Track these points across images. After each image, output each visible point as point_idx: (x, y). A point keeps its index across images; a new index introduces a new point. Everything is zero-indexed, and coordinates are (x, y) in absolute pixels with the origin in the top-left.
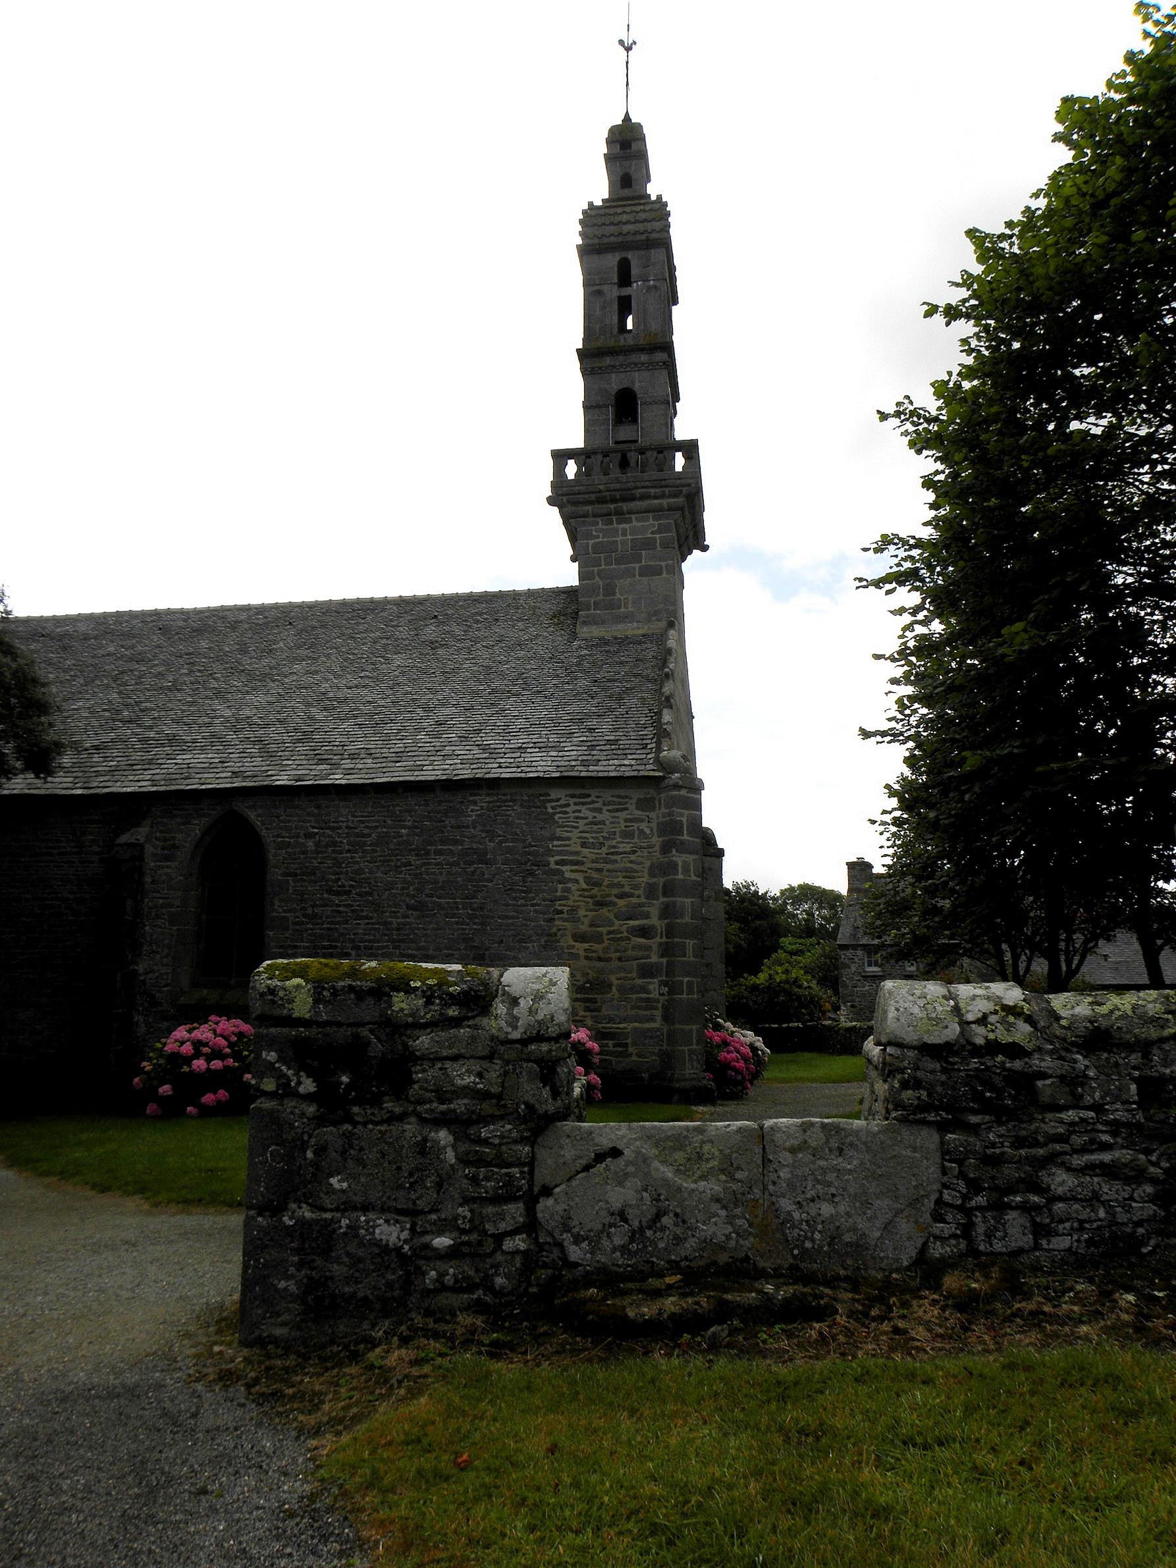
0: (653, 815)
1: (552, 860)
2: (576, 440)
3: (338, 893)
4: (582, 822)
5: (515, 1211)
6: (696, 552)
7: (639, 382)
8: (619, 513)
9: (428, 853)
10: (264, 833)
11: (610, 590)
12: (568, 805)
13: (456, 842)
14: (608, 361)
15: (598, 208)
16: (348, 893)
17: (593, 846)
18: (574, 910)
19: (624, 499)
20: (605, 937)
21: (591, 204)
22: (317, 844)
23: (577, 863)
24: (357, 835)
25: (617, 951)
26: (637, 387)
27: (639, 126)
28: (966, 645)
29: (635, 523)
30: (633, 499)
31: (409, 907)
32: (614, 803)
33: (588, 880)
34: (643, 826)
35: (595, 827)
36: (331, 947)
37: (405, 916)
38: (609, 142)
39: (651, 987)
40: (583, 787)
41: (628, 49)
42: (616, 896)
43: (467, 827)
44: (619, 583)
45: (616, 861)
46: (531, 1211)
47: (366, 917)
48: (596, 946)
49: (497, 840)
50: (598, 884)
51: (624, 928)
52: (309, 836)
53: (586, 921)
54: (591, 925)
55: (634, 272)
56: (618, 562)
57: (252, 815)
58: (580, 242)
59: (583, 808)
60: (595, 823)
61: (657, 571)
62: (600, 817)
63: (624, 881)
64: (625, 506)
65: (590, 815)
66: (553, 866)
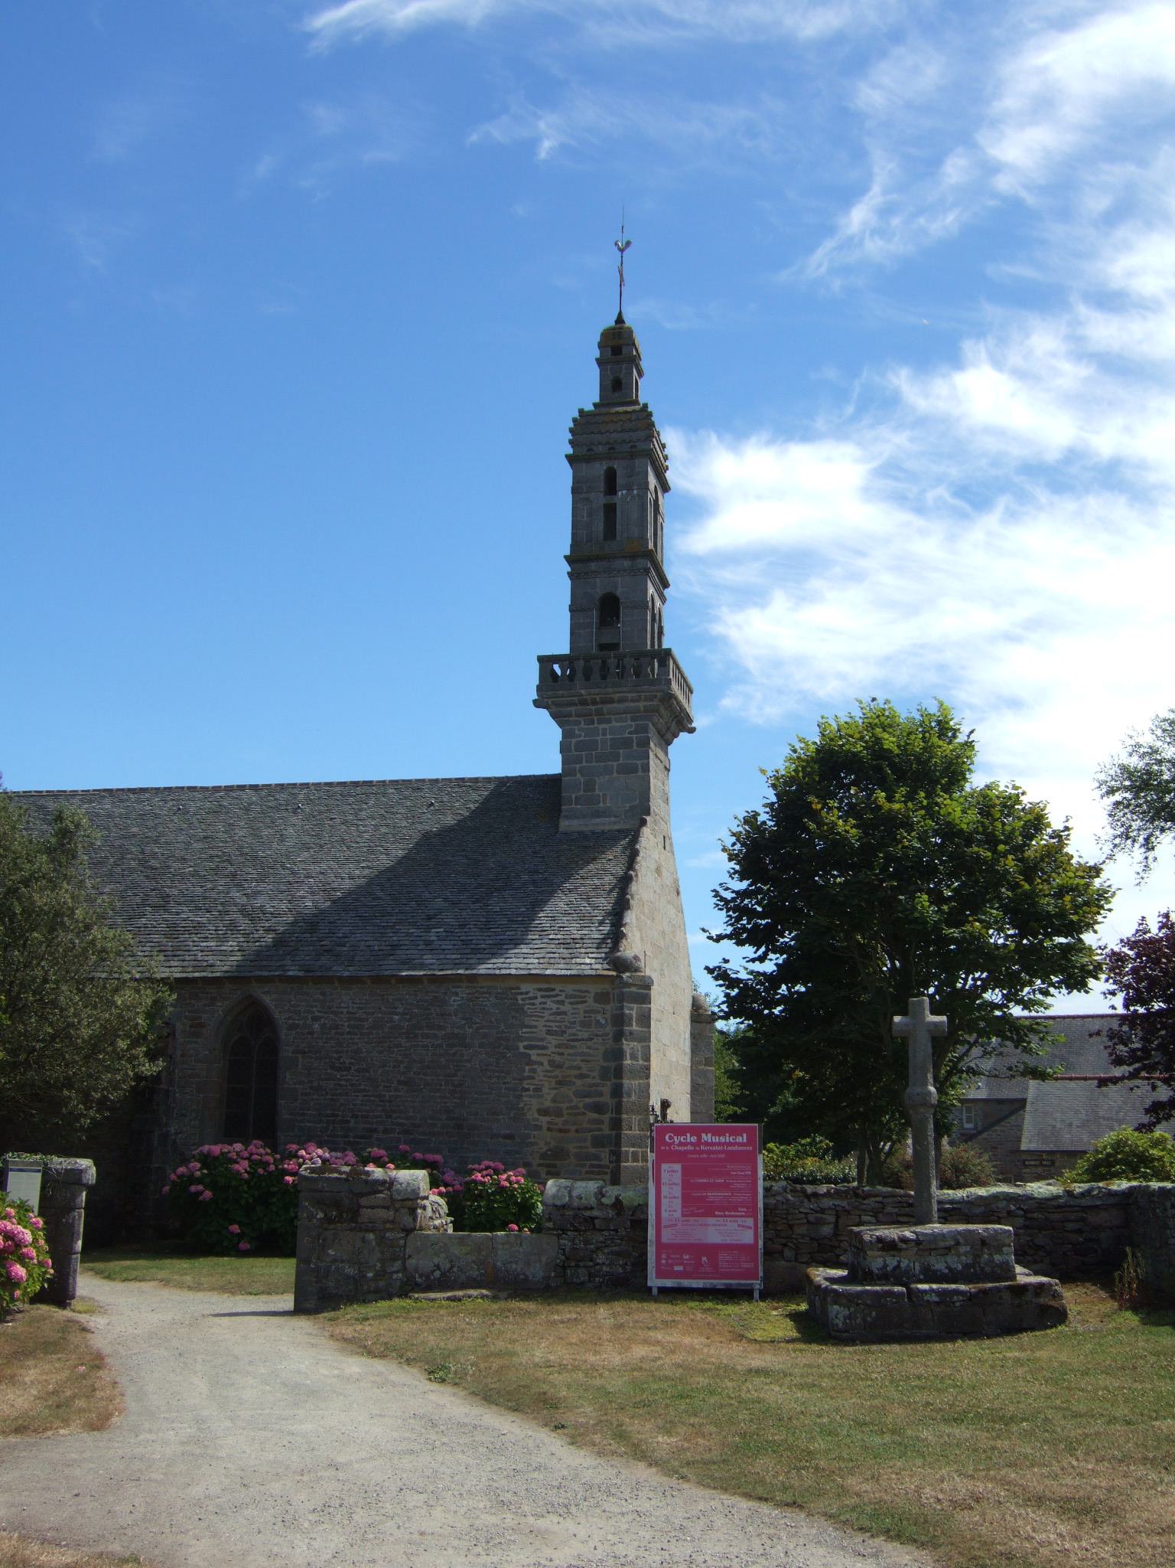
0: (608, 1007)
1: (521, 1045)
2: (563, 648)
3: (339, 1069)
4: (547, 1013)
5: (398, 1264)
6: (683, 735)
8: (599, 713)
11: (590, 786)
13: (440, 1028)
14: (593, 566)
16: (348, 1069)
17: (556, 1033)
18: (538, 1089)
19: (603, 702)
20: (565, 1112)
21: (581, 411)
23: (544, 1048)
26: (619, 592)
27: (630, 331)
29: (614, 724)
30: (612, 701)
31: (399, 1082)
32: (574, 997)
33: (551, 1063)
34: (599, 1017)
35: (558, 1018)
37: (396, 1090)
41: (622, 251)
43: (449, 1015)
46: (404, 1264)
48: (557, 1120)
50: (559, 1066)
51: (581, 1105)
54: (554, 1101)
55: (619, 481)
57: (267, 999)
58: (570, 451)
59: (549, 1001)
60: (559, 1014)
62: (562, 1008)
63: (582, 1065)
64: (606, 708)
65: (554, 1006)
66: (522, 1050)
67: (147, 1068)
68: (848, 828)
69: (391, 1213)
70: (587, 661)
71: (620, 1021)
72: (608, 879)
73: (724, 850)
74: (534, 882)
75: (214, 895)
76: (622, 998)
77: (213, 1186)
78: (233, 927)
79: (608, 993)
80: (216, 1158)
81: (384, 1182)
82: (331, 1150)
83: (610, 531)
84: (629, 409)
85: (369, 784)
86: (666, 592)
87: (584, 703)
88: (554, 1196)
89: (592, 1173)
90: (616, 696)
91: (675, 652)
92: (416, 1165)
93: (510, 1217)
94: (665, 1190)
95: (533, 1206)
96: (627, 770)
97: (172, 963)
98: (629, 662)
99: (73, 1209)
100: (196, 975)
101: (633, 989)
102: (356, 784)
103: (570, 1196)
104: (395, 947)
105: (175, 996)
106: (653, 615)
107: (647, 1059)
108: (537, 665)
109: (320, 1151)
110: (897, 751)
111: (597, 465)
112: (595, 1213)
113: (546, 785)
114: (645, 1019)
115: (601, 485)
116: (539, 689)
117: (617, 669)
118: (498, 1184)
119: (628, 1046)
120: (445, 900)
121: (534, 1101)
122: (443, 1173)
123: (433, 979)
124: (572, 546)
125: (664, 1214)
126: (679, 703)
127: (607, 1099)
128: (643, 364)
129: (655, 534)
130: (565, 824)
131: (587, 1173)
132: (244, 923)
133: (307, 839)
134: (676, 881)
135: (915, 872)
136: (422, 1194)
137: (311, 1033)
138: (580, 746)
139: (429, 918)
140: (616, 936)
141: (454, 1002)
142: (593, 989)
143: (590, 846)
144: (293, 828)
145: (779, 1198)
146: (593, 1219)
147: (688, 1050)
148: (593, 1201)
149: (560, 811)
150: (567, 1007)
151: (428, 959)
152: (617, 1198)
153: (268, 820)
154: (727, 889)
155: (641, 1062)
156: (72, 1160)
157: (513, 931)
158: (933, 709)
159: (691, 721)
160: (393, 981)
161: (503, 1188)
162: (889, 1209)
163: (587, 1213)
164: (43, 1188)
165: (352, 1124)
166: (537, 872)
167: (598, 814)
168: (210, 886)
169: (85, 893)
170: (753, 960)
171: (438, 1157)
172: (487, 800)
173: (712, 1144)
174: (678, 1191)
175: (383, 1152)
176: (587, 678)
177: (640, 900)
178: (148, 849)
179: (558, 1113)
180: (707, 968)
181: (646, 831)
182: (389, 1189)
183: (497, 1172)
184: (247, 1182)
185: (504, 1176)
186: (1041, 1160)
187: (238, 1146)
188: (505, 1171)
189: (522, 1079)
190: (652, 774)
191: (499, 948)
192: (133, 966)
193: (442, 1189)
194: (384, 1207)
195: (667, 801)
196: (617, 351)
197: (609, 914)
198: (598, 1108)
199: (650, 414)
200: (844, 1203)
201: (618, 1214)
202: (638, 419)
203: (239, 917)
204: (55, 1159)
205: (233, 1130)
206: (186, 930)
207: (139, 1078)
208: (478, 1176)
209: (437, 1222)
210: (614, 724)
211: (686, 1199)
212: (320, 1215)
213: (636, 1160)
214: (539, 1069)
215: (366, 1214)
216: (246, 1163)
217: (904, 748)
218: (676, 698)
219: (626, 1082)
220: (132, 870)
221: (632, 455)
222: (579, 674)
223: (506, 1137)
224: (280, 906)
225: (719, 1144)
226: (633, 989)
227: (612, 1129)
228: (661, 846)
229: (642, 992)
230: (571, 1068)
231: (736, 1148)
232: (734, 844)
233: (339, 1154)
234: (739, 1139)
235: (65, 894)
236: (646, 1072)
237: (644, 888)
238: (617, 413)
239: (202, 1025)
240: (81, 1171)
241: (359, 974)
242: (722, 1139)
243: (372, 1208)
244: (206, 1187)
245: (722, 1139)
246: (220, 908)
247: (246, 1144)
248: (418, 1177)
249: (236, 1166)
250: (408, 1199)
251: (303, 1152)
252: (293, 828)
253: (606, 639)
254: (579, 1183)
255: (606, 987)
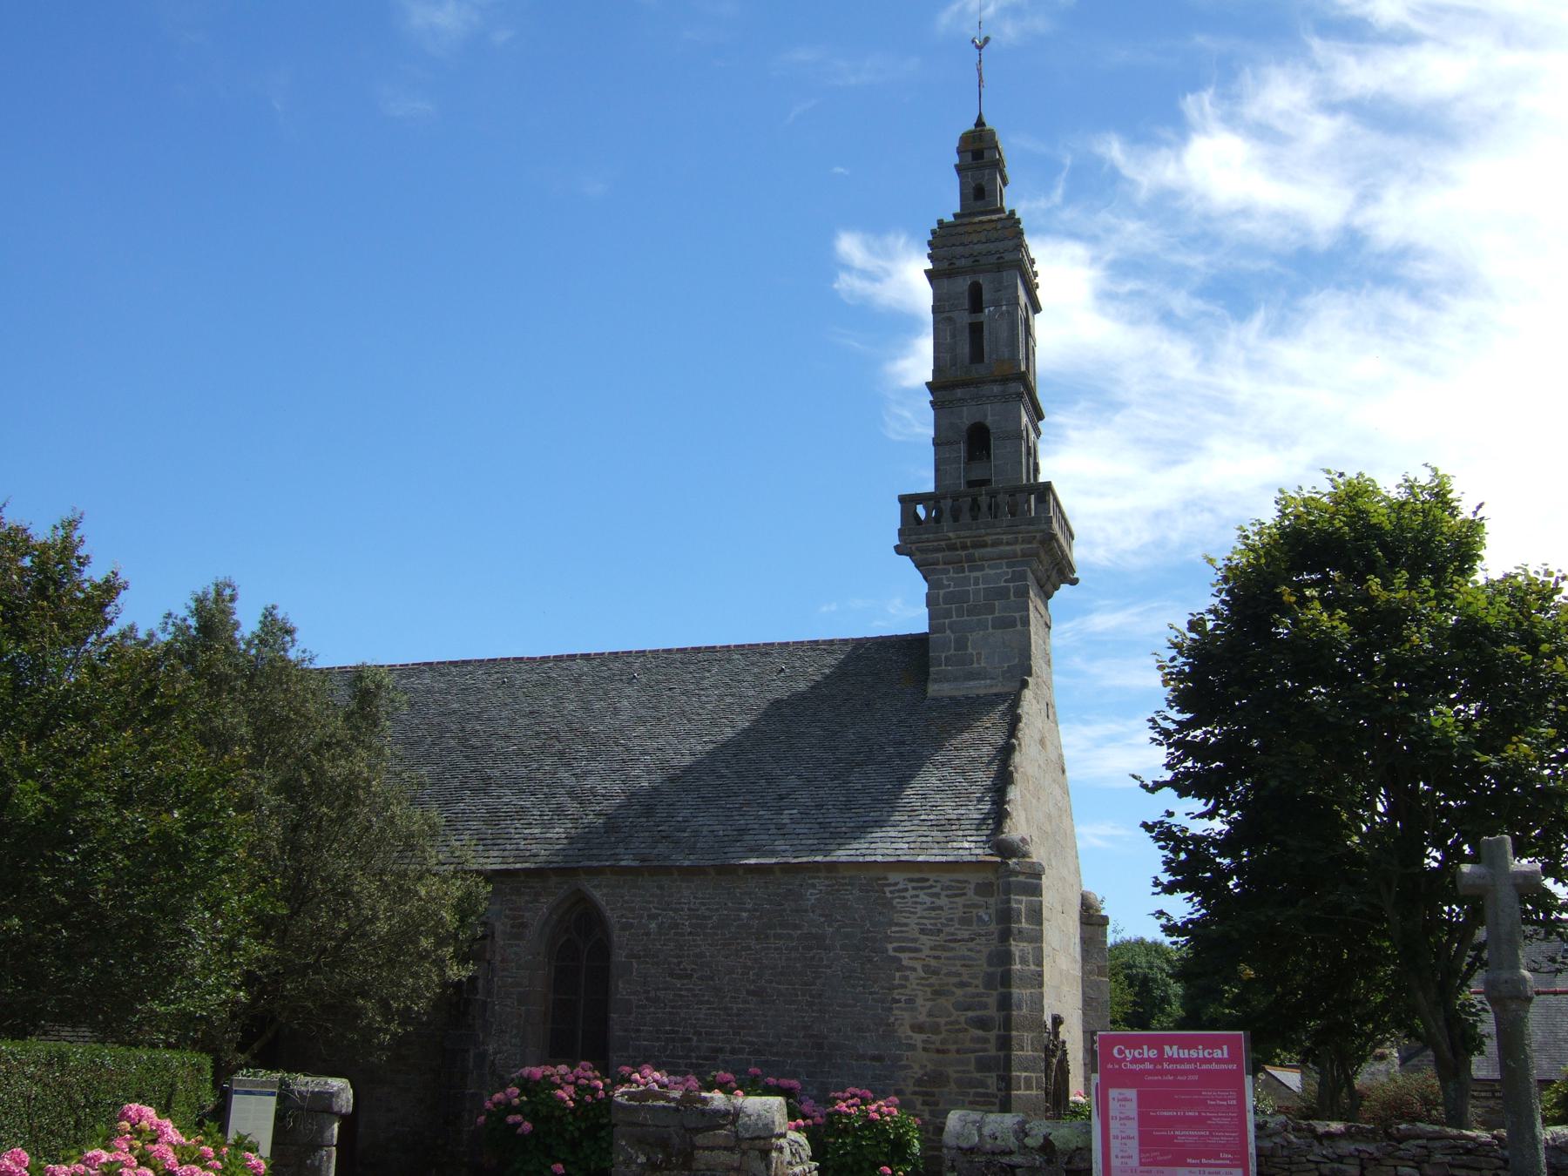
0: (992, 901)
1: (890, 947)
3: (680, 977)
7: (991, 416)
8: (970, 559)
9: (767, 937)
10: (608, 914)
11: (961, 644)
12: (906, 890)
13: (796, 927)
14: (959, 392)
15: (950, 225)
18: (910, 1001)
19: (976, 546)
20: (943, 1028)
21: (940, 222)
22: (660, 926)
23: (917, 950)
24: (698, 917)
25: (955, 1042)
26: (989, 421)
27: (992, 133)
28: (1358, 681)
30: (985, 545)
31: (749, 993)
33: (926, 968)
34: (981, 913)
35: (933, 914)
36: (673, 1032)
38: (960, 151)
39: (989, 1082)
40: (921, 871)
41: (979, 48)
42: (955, 985)
44: (972, 637)
45: (953, 949)
47: (708, 1002)
49: (836, 925)
50: (936, 972)
51: (962, 1019)
52: (652, 917)
53: (924, 1011)
54: (930, 1015)
55: (986, 296)
56: (970, 612)
58: (930, 266)
60: (933, 909)
61: (1012, 624)
62: (938, 902)
63: (963, 970)
64: (977, 553)
65: (928, 900)
66: (891, 953)
67: (455, 972)
68: (1336, 625)
69: (737, 1157)
70: (955, 498)
71: (1006, 916)
72: (986, 749)
73: (1161, 668)
74: (901, 755)
75: (539, 775)
76: (1008, 889)
77: (533, 1116)
78: (560, 811)
79: (991, 884)
80: (537, 1082)
81: (727, 1113)
82: (670, 1073)
83: (977, 354)
84: (994, 217)
85: (712, 649)
86: (1041, 424)
87: (952, 548)
88: (958, 1136)
89: (977, 1103)
90: (989, 539)
91: (1056, 487)
92: (769, 1091)
93: (882, 1158)
94: (1115, 1127)
95: (909, 1144)
96: (1005, 624)
97: (492, 853)
98: (1002, 498)
99: (321, 1147)
100: (518, 866)
101: (1021, 878)
102: (697, 650)
103: (981, 1135)
104: (743, 831)
105: (490, 888)
106: (1028, 448)
107: (1040, 964)
108: (899, 506)
109: (657, 1075)
110: (1389, 527)
111: (960, 280)
112: (1017, 1159)
113: (910, 650)
114: (1036, 915)
115: (966, 304)
116: (901, 533)
117: (985, 512)
118: (865, 1116)
119: (1017, 947)
120: (799, 777)
121: (906, 1015)
122: (801, 1102)
123: (787, 868)
124: (934, 371)
125: (1115, 1162)
126: (1060, 546)
127: (992, 1012)
128: (1007, 171)
129: (1027, 358)
130: (933, 689)
131: (971, 1103)
132: (572, 807)
133: (643, 712)
134: (1061, 756)
135: (1429, 680)
136: (777, 1130)
137: (648, 934)
138: (949, 598)
139: (781, 798)
140: (999, 814)
141: (811, 896)
142: (975, 878)
143: (964, 712)
144: (628, 700)
145: (1277, 1140)
146: (1013, 1167)
147: (1079, 958)
148: (1012, 1142)
149: (927, 673)
150: (943, 901)
151: (780, 845)
152: (1046, 1138)
153: (600, 692)
154: (1166, 718)
155: (1033, 967)
156: (322, 1080)
157: (877, 809)
158: (1424, 478)
159: (1073, 571)
160: (741, 872)
161: (873, 1121)
162: (1438, 1157)
163: (1005, 1160)
164: (280, 1117)
165: (694, 1043)
166: (903, 743)
167: (972, 676)
168: (535, 766)
169: (384, 769)
170: (1202, 816)
171: (794, 1083)
172: (844, 663)
173: (1180, 1061)
174: (1133, 1128)
175: (729, 1076)
176: (956, 519)
177: (1025, 774)
178: (469, 727)
179: (935, 1029)
180: (1145, 825)
181: (1028, 694)
182: (734, 1123)
183: (864, 1101)
184: (573, 1111)
185: (874, 1107)
186: (1493, 1092)
187: (563, 1069)
188: (874, 1101)
189: (892, 988)
190: (1032, 629)
191: (861, 830)
192: (445, 856)
193: (801, 1122)
194: (725, 1148)
195: (1048, 663)
196: (978, 155)
197: (988, 790)
198: (983, 1024)
199: (1018, 222)
200: (1371, 1148)
201: (1049, 1161)
202: (1004, 228)
203: (565, 799)
204: (301, 1078)
205: (560, 1050)
206: (508, 816)
207: (445, 984)
208: (842, 1106)
209: (798, 1169)
210: (987, 571)
211: (1146, 1140)
212: (642, 1159)
213: (1029, 1087)
214: (912, 976)
215: (703, 1156)
216: (571, 1089)
217: (1399, 526)
218: (1057, 541)
219: (1015, 991)
220: (450, 750)
221: (1000, 267)
222: (947, 515)
223: (874, 1058)
224: (608, 786)
225: (1189, 1060)
226: (1021, 878)
227: (999, 1049)
228: (1044, 714)
229: (1032, 882)
230: (948, 974)
231: (1214, 1066)
232: (1173, 659)
233: (679, 1079)
234: (1218, 1054)
235: (360, 763)
236: (1038, 980)
237: (1026, 760)
238: (981, 222)
239: (523, 925)
240: (332, 1094)
241: (702, 863)
242: (1194, 1054)
243: (712, 1149)
244: (525, 1116)
245: (1194, 1054)
246: (546, 790)
247: (572, 1065)
248: (767, 1107)
249: (559, 1092)
250: (758, 1138)
251: (636, 1076)
252: (628, 700)
253: (978, 473)
254: (992, 1117)
255: (990, 876)
